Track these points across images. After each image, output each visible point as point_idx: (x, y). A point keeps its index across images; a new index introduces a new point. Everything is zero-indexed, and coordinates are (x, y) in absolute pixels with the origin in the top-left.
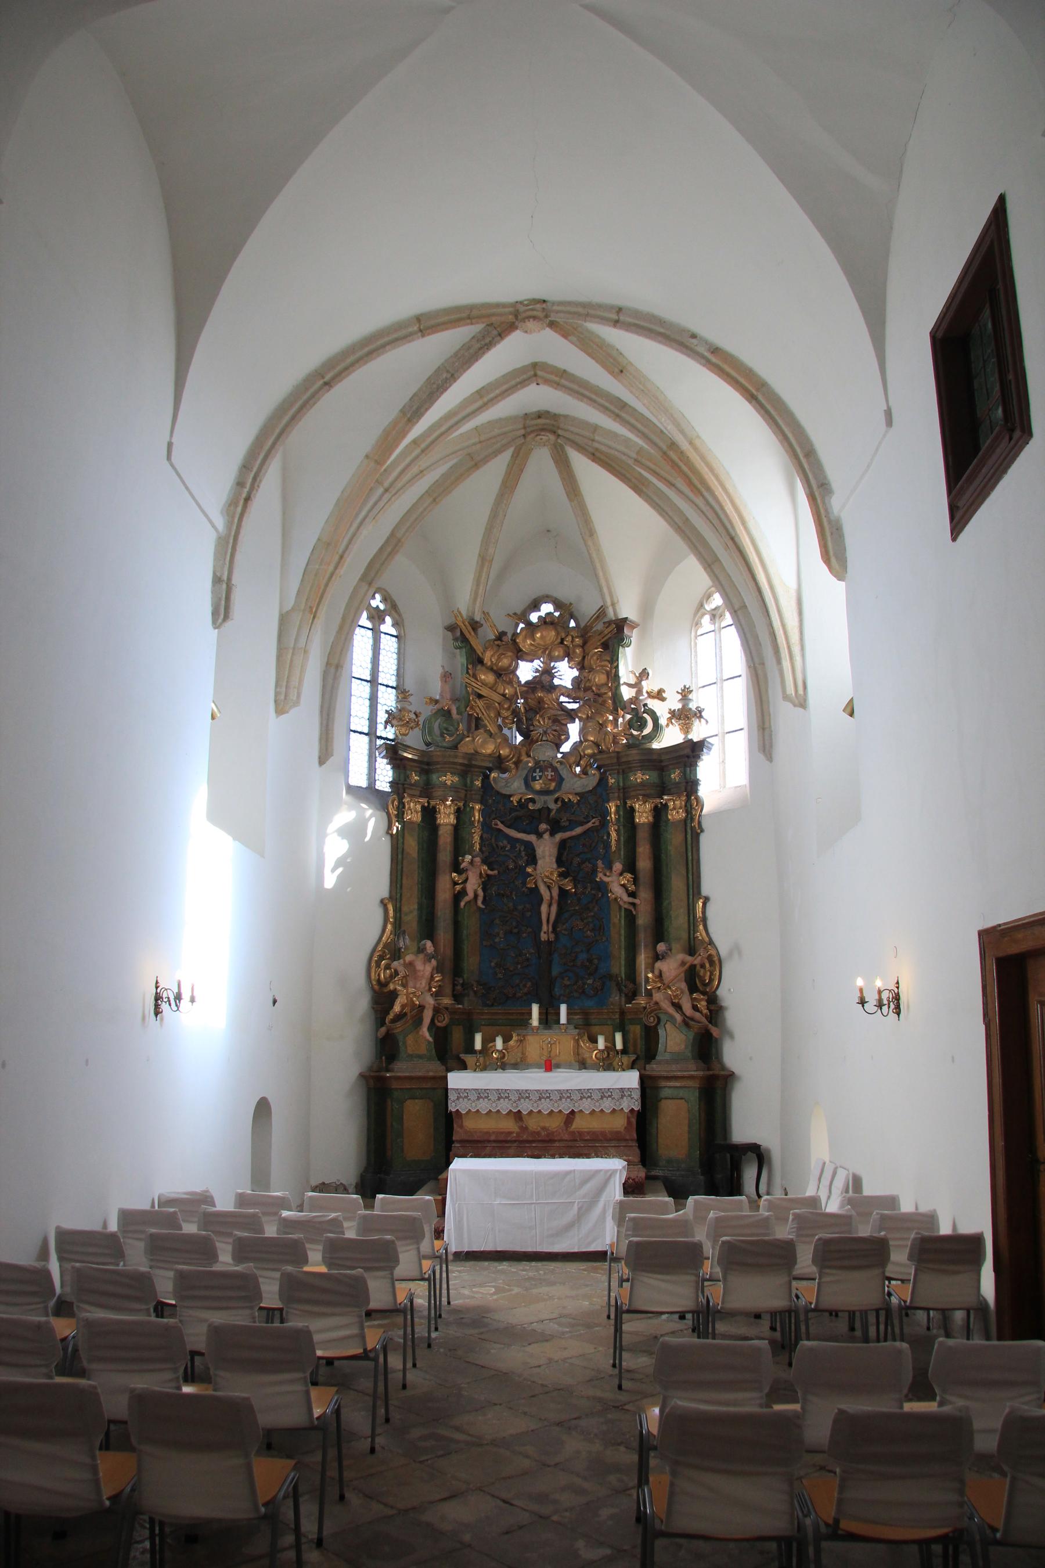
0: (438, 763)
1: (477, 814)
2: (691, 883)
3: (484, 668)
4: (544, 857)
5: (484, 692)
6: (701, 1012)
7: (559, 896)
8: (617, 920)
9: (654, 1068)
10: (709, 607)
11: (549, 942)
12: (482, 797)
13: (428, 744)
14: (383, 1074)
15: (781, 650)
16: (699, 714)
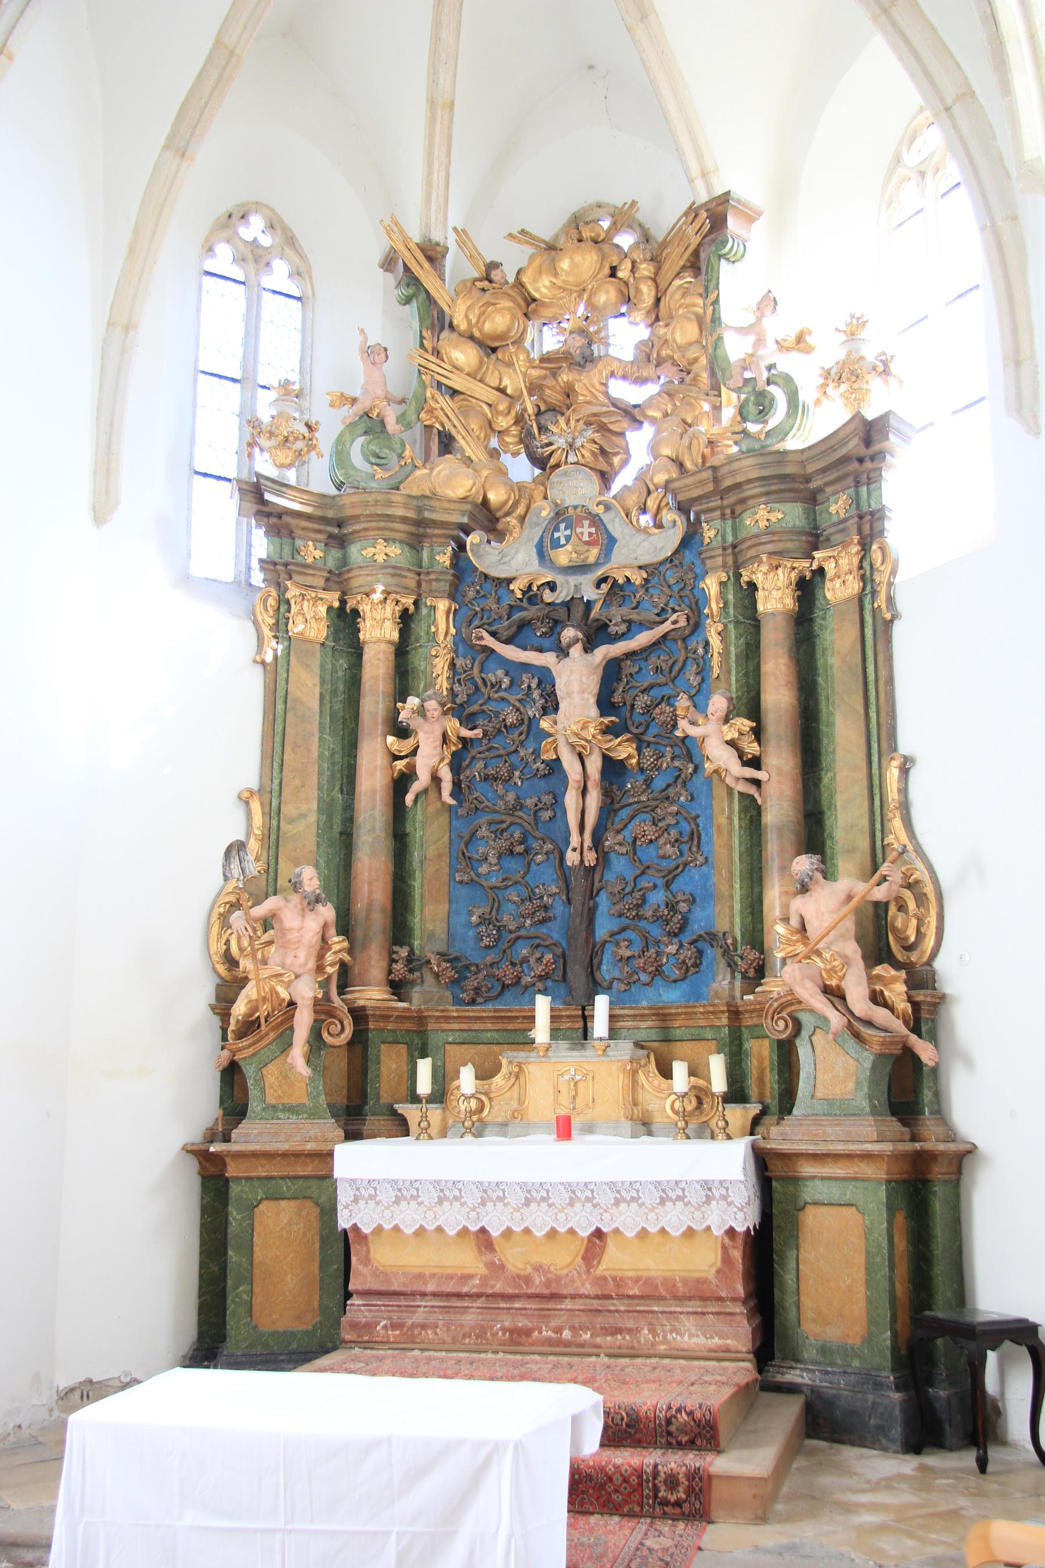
0: (356, 518)
3: (454, 336)
5: (457, 382)
6: (891, 1009)
10: (912, 159)
13: (339, 486)
15: (1010, 47)
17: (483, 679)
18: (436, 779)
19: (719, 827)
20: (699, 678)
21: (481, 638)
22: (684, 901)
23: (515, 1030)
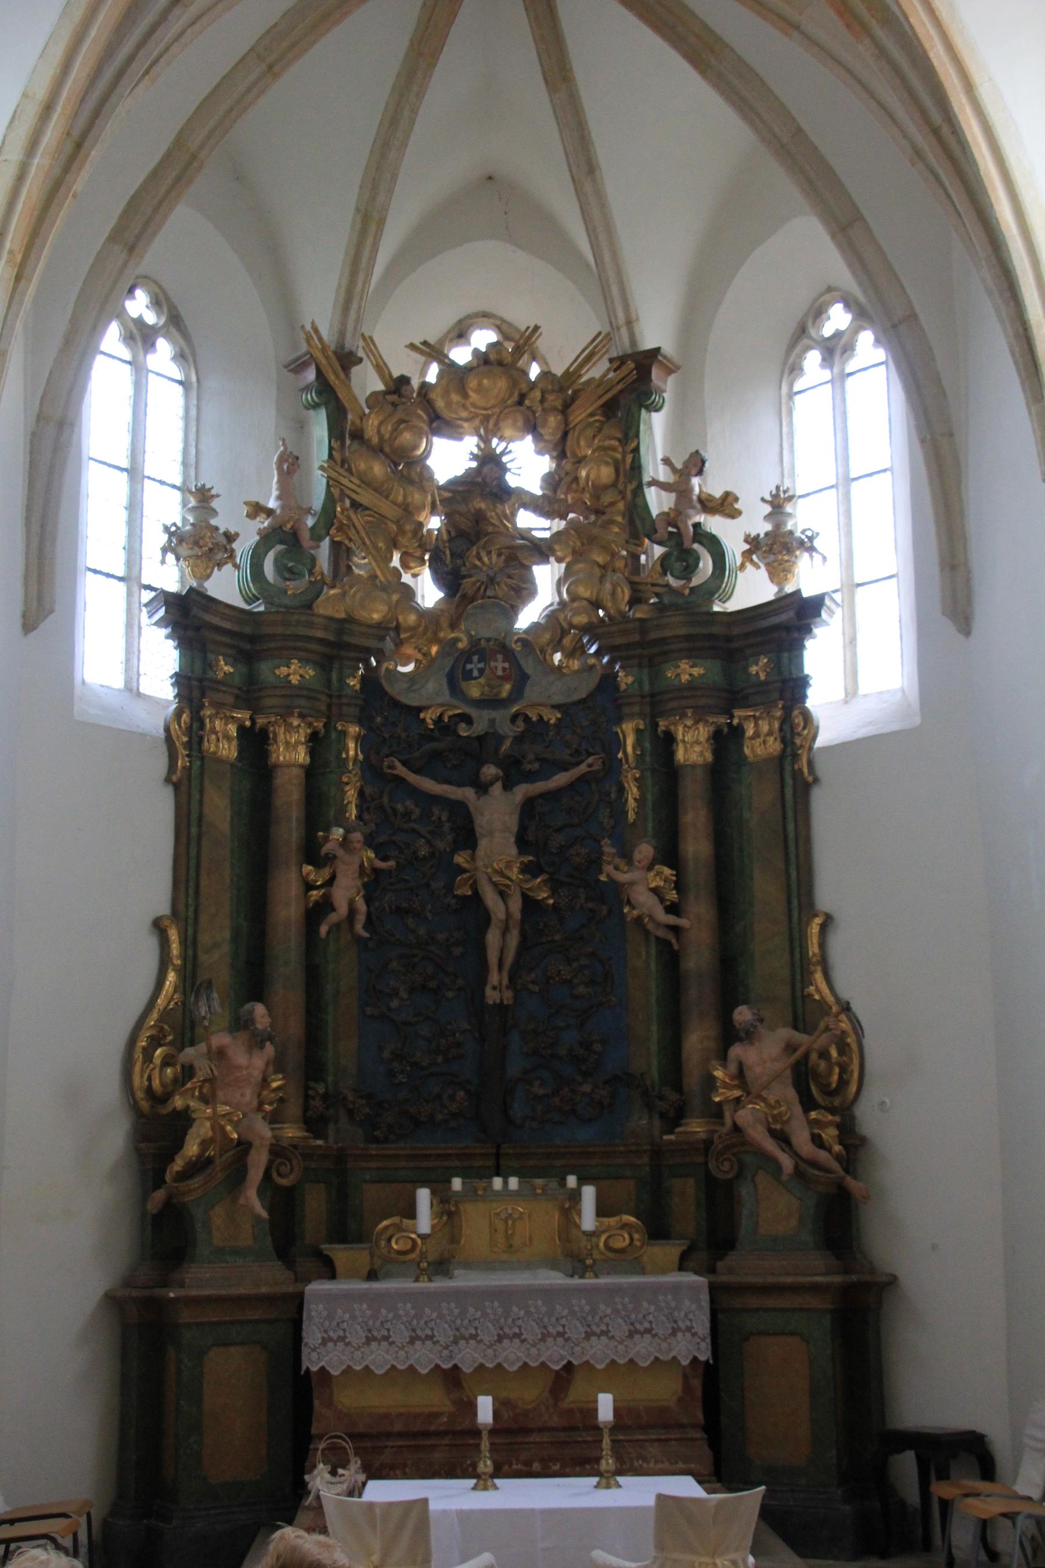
0: (272, 637)
1: (352, 745)
2: (794, 887)
5: (365, 497)
6: (829, 1150)
7: (524, 911)
8: (642, 964)
9: (743, 1266)
11: (501, 1007)
14: (158, 1292)
16: (807, 545)
20: (612, 822)
21: (392, 767)
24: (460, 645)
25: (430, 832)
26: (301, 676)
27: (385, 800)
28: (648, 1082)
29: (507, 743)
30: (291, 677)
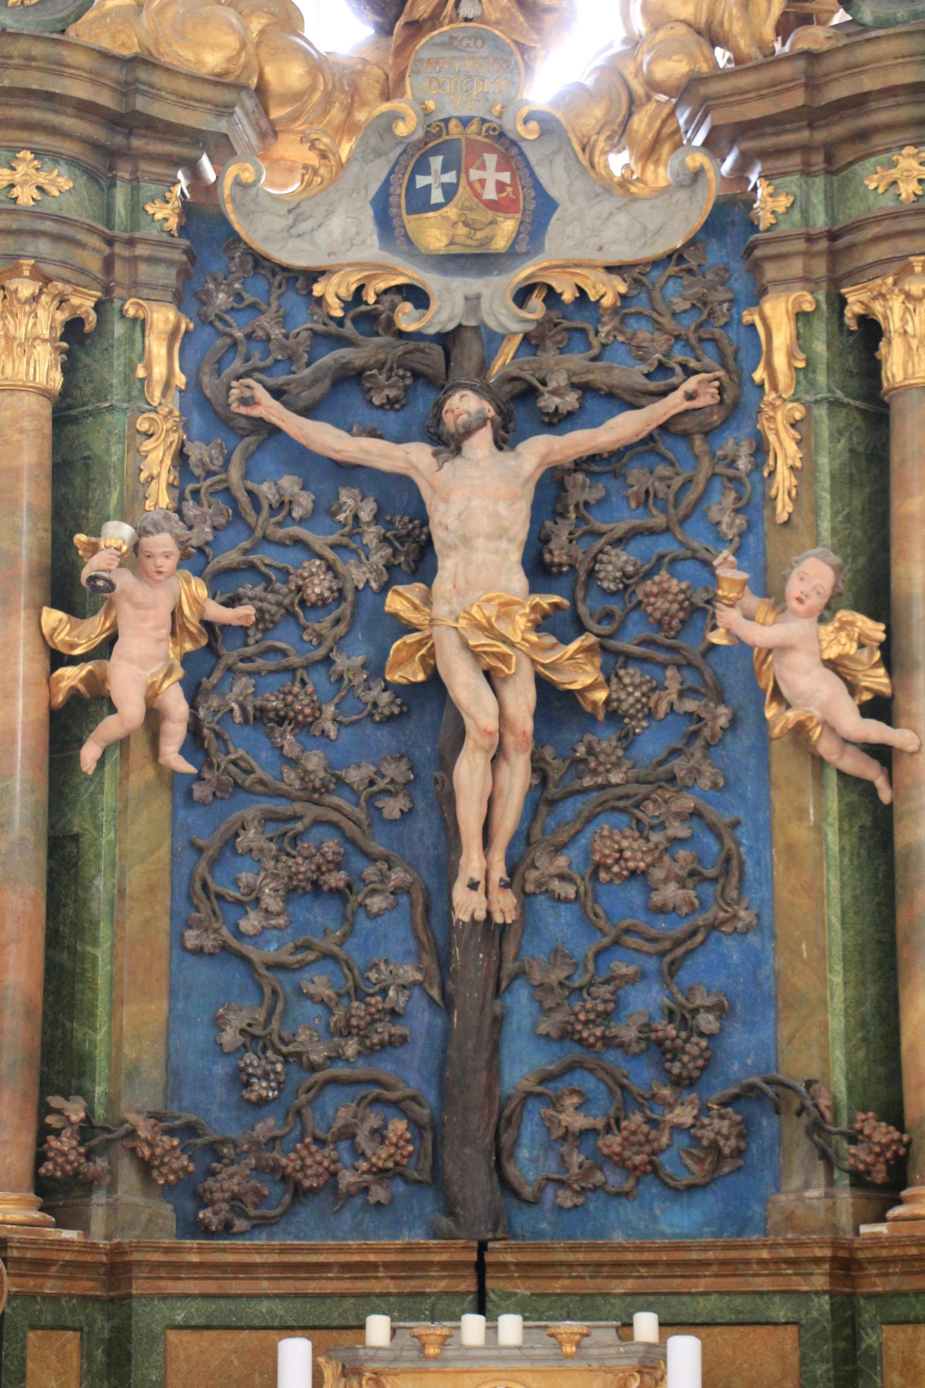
4: (466, 541)
8: (809, 837)
11: (490, 930)
12: (185, 274)
17: (250, 493)
18: (154, 717)
19: (790, 848)
20: (740, 521)
22: (708, 1009)
23: (323, 1296)
24: (402, 129)
25: (333, 547)
26: (40, 188)
27: (235, 474)
28: (824, 1102)
29: (509, 350)
30: (16, 192)
